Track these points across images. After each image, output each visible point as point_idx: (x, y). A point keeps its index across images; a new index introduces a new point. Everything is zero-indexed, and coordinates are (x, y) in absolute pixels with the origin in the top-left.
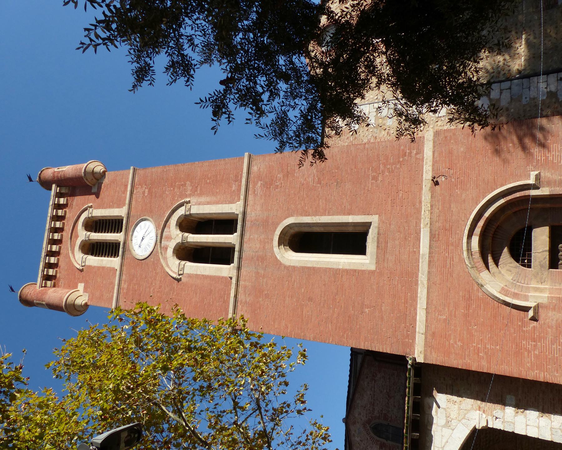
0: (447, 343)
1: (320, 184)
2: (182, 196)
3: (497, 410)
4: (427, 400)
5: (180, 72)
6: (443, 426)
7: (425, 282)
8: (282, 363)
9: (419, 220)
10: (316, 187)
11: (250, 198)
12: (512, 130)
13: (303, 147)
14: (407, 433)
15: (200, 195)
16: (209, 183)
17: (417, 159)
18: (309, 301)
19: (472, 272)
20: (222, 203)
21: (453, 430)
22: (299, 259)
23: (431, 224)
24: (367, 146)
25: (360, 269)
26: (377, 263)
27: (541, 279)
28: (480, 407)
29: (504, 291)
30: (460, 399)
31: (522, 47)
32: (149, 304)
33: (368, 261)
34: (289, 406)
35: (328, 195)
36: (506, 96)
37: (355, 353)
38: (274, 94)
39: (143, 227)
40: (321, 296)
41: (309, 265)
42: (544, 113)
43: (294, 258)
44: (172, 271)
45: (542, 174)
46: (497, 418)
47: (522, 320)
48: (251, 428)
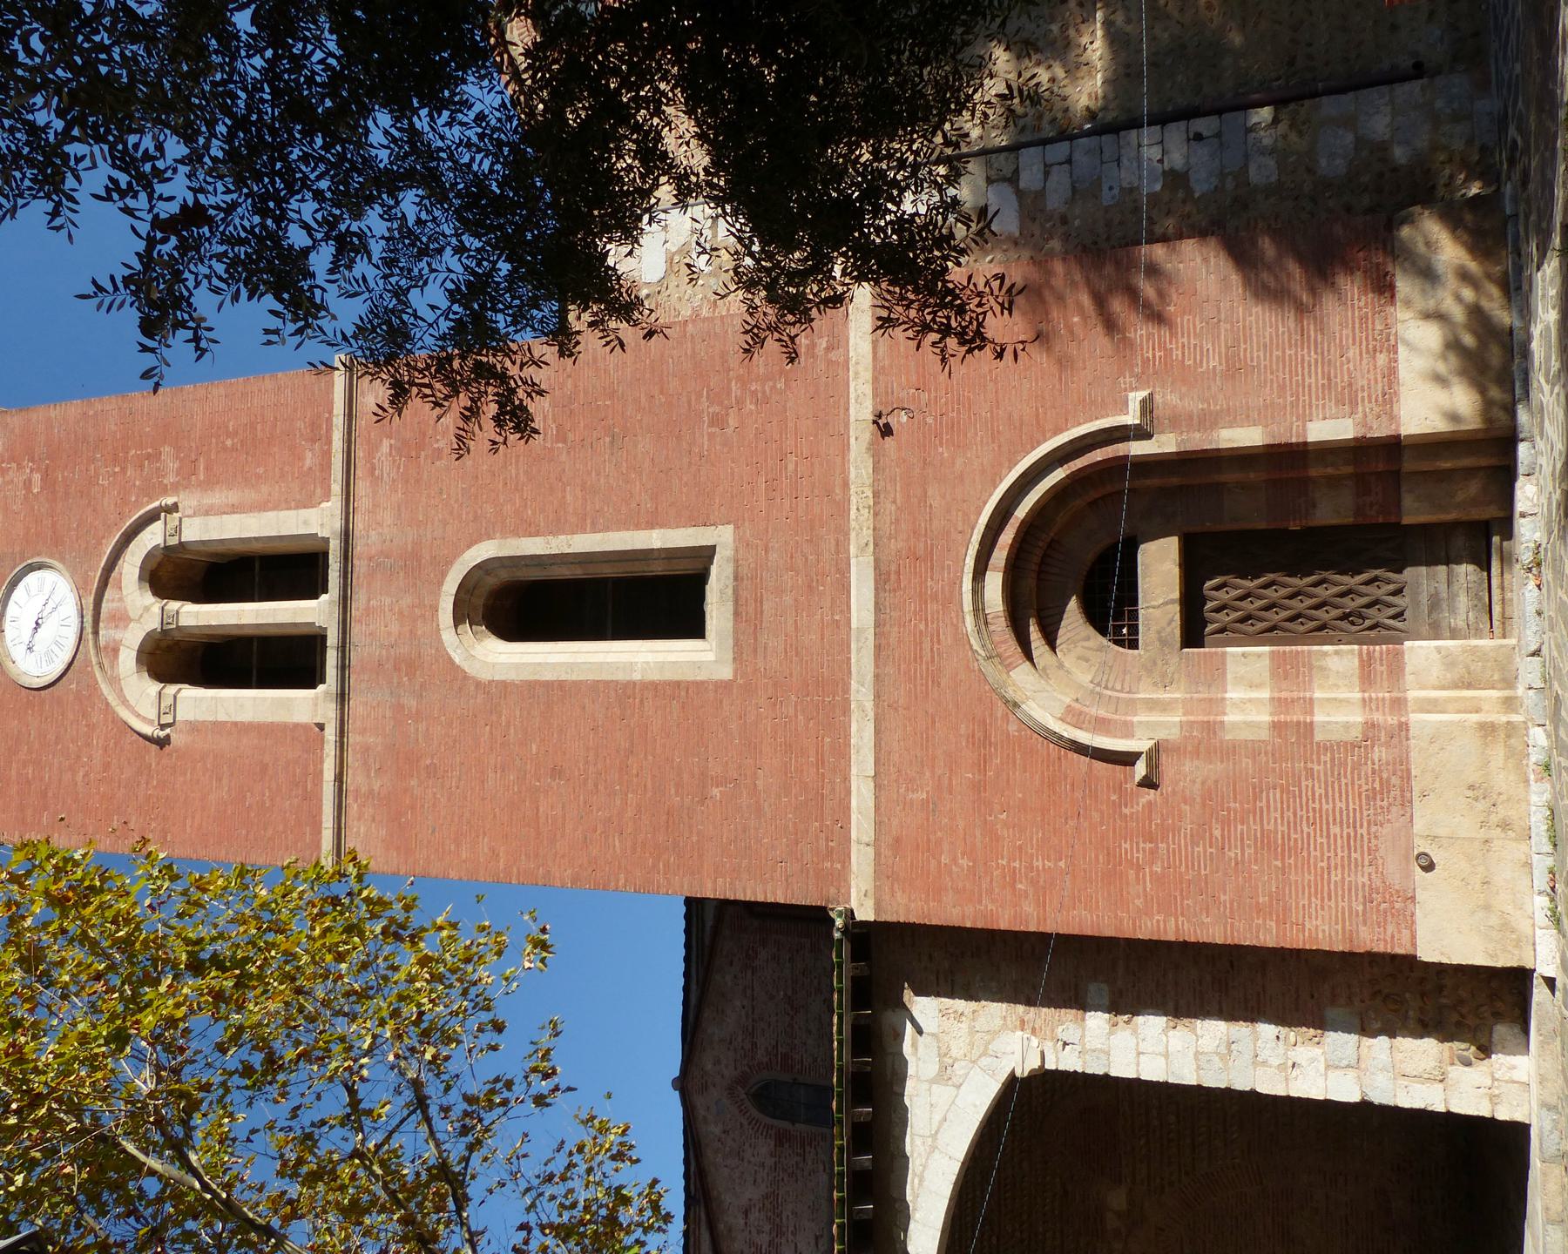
0: (933, 863)
1: (565, 442)
2: (149, 492)
3: (1065, 1022)
4: (890, 1017)
5: (27, 183)
6: (933, 1081)
7: (869, 705)
8: (482, 972)
9: (843, 532)
10: (552, 449)
11: (362, 487)
12: (1078, 277)
13: (464, 400)
14: (839, 1110)
15: (209, 484)
16: (234, 449)
17: (829, 362)
18: (553, 777)
19: (990, 669)
20: (275, 508)
21: (959, 1087)
22: (516, 659)
23: (876, 545)
24: (690, 326)
25: (691, 678)
26: (737, 658)
27: (1163, 675)
28: (1023, 1022)
29: (1073, 716)
30: (973, 1005)
31: (1095, 45)
32: (59, 841)
33: (711, 657)
34: (509, 1085)
35: (589, 473)
36: (1059, 182)
37: (694, 907)
38: (348, 247)
39: (33, 592)
40: (587, 762)
41: (548, 676)
42: (1158, 230)
43: (503, 659)
44: (138, 716)
45: (1157, 398)
46: (1065, 1044)
47: (1119, 789)
48: (408, 1155)
